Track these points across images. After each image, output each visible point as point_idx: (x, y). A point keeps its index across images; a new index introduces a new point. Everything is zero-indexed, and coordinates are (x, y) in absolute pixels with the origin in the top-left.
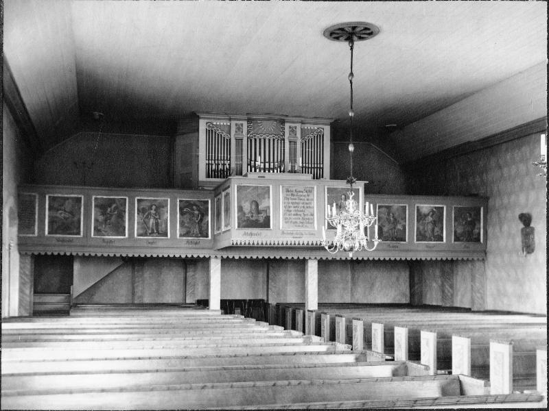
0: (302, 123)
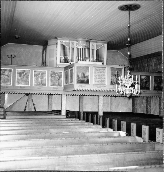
0: (97, 42)
